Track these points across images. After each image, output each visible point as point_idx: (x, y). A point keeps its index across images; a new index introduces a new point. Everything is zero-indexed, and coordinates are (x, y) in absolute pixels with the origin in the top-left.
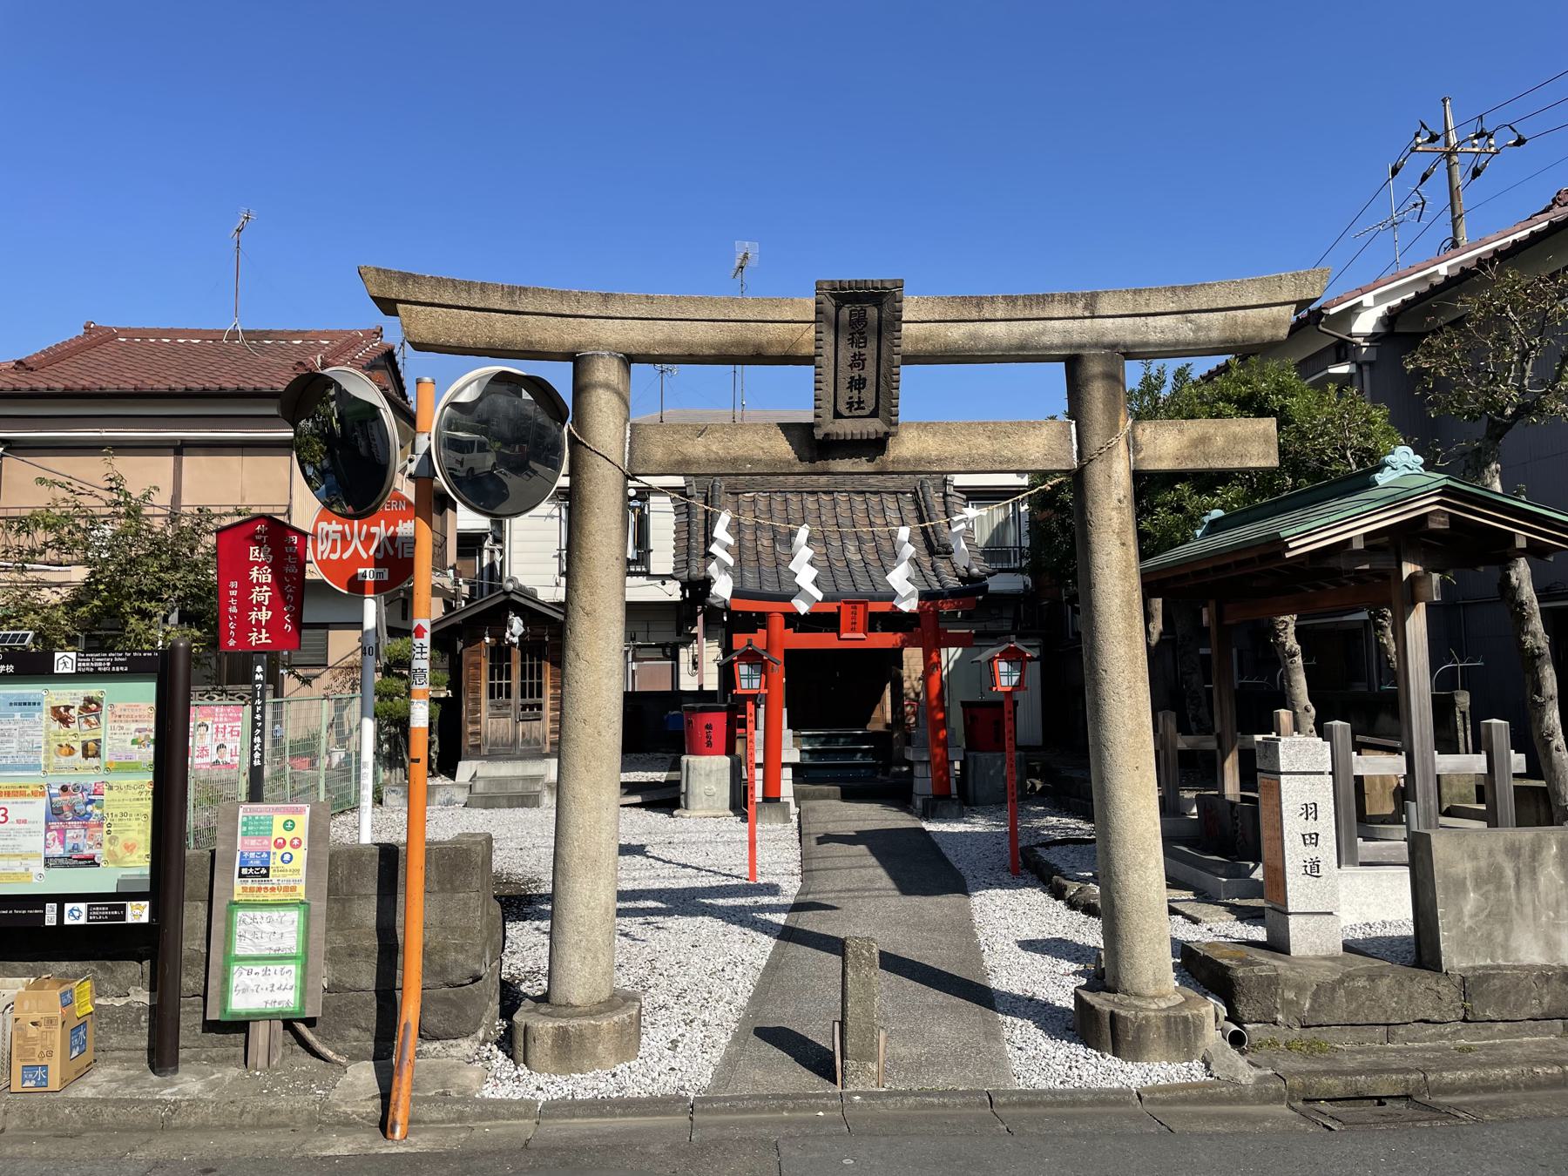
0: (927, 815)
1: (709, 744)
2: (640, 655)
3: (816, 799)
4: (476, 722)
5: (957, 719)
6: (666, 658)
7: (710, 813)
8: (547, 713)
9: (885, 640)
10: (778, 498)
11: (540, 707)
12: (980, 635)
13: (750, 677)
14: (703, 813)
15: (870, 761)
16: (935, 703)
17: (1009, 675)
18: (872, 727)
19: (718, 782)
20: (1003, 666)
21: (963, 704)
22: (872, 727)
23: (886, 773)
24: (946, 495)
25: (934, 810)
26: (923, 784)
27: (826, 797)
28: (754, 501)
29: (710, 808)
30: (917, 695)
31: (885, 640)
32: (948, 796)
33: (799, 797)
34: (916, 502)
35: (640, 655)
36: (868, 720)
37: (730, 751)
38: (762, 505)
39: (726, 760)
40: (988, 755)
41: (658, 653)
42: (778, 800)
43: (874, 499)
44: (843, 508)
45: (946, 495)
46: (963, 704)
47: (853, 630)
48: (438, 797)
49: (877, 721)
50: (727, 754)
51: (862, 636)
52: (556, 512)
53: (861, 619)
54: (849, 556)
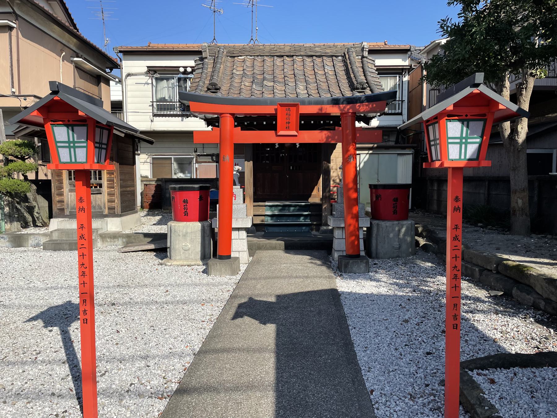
0: (345, 266)
1: (186, 214)
2: (199, 160)
3: (267, 249)
4: (61, 194)
5: (365, 195)
6: (213, 161)
7: (185, 263)
8: (105, 189)
9: (316, 137)
10: (259, 59)
11: (101, 186)
12: (378, 148)
13: (71, 145)
14: (181, 263)
15: (308, 222)
16: (351, 185)
17: (463, 142)
18: (312, 200)
19: (192, 241)
20: (454, 128)
21: (370, 186)
22: (312, 200)
23: (318, 230)
24: (363, 57)
25: (346, 266)
26: (340, 244)
27: (274, 248)
28: (244, 61)
29: (187, 259)
30: (340, 180)
31: (316, 137)
32: (358, 256)
33: (252, 250)
34: (344, 61)
35: (199, 160)
36: (310, 196)
37: (203, 218)
38: (248, 63)
39: (197, 226)
40: (388, 223)
41: (209, 159)
42: (229, 257)
43: (318, 60)
44: (313, 92)
45: (363, 57)
46: (370, 186)
47: (288, 129)
48: (30, 242)
49: (315, 196)
50: (200, 220)
51: (294, 133)
52: (150, 81)
53: (294, 120)
54: (298, 91)
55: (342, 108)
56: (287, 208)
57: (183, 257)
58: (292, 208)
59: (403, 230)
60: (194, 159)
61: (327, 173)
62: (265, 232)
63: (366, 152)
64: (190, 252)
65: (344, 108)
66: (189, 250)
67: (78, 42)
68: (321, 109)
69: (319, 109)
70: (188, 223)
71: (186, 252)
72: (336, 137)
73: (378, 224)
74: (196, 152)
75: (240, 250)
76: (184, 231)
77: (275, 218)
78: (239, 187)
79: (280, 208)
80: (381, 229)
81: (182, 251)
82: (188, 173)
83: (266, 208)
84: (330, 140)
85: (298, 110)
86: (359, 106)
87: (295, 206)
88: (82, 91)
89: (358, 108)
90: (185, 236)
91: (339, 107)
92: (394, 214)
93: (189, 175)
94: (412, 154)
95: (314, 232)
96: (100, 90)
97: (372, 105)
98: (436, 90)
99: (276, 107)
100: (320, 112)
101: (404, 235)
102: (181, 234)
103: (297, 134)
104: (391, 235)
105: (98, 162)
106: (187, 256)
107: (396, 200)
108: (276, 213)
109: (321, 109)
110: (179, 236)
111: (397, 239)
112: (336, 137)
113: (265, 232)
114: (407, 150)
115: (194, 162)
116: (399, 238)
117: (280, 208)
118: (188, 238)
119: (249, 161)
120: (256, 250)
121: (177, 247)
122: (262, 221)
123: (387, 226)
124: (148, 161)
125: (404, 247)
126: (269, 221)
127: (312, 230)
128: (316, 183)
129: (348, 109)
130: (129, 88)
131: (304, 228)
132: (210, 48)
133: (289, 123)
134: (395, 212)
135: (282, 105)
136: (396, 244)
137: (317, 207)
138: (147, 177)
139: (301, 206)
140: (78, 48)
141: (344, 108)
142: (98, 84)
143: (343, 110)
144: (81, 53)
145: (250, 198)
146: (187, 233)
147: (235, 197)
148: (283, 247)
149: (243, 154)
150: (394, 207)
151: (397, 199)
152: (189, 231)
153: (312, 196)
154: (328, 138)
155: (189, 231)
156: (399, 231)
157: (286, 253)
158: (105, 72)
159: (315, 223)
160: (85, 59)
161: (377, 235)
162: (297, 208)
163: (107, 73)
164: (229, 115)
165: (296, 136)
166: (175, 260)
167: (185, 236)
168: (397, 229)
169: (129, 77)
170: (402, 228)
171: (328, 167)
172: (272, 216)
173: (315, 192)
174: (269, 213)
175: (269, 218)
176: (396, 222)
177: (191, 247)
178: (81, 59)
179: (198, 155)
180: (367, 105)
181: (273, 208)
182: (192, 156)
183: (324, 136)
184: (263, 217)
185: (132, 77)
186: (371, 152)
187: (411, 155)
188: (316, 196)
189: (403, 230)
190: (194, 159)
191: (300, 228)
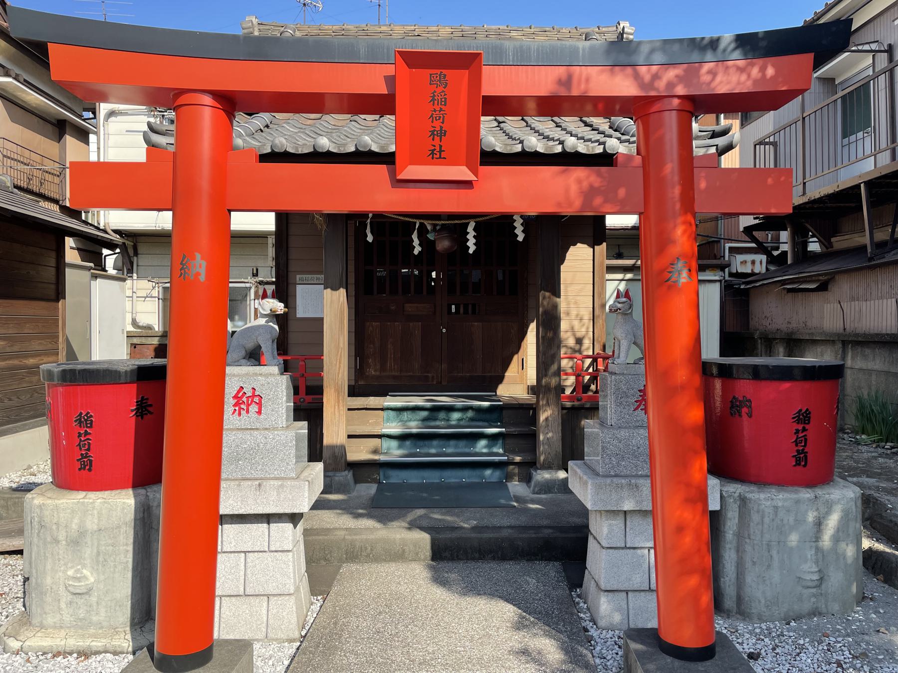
3: (377, 559)
7: (73, 643)
14: (57, 641)
19: (100, 561)
23: (527, 479)
27: (398, 556)
29: (81, 625)
33: (322, 567)
36: (500, 379)
47: (437, 156)
51: (462, 173)
55: (647, 78)
56: (442, 415)
57: (67, 618)
58: (456, 416)
59: (833, 521)
60: (252, 291)
61: (550, 323)
62: (379, 483)
63: (620, 276)
64: (94, 599)
65: (656, 77)
66: (89, 592)
67: (12, 50)
68: (567, 82)
69: (560, 82)
70: (92, 495)
71: (80, 601)
72: (622, 192)
73: (743, 501)
74: (255, 275)
75: (271, 590)
76: (74, 526)
77: (408, 443)
78: (275, 370)
79: (425, 414)
80: (755, 517)
81: (65, 597)
82: (240, 320)
83: (385, 413)
84: (598, 201)
85: (476, 81)
86: (713, 73)
87: (465, 409)
88: (351, 268)
89: (706, 78)
90: (76, 542)
91: (637, 77)
92: (798, 464)
93: (240, 323)
94: (720, 281)
95: (516, 487)
96: (63, 150)
97: (763, 69)
98: (770, 143)
99: (390, 70)
100: (563, 92)
101: (836, 539)
102: (62, 536)
103: (470, 177)
104: (793, 539)
105: (464, 313)
106: (82, 613)
107: (804, 418)
108: (414, 427)
109: (567, 82)
110: (56, 541)
111: (810, 553)
112: (622, 192)
113: (379, 483)
114: (708, 272)
115: (253, 297)
116: (818, 549)
117: (425, 414)
118: (88, 552)
119: (335, 288)
120: (341, 561)
121: (49, 581)
122: (375, 452)
123: (776, 508)
124: (155, 293)
125: (835, 579)
126: (394, 452)
127: (509, 477)
128: (517, 348)
129: (670, 85)
130: (112, 140)
131: (488, 472)
132: (262, 27)
133: (442, 133)
134: (801, 459)
135: (414, 60)
136: (809, 570)
137: (521, 416)
138: (149, 328)
139: (479, 410)
140: (10, 59)
141: (656, 77)
142: (60, 137)
143: (651, 85)
144: (16, 70)
145: (338, 391)
146: (82, 533)
147: (260, 404)
148: (427, 551)
149: (320, 273)
150: (796, 443)
151: (808, 413)
152: (91, 524)
153: (506, 380)
154: (589, 194)
155: (91, 524)
156: (819, 524)
157: (439, 580)
158: (80, 116)
159: (518, 459)
160: (27, 83)
161: (740, 536)
162: (470, 414)
163: (84, 120)
164: (207, 100)
165: (468, 184)
166: (42, 627)
167: (76, 542)
168: (811, 517)
169: (112, 119)
170: (828, 513)
171: (555, 307)
172: (402, 438)
173: (512, 372)
174: (394, 429)
175: (394, 443)
176: (806, 494)
177: (98, 581)
178: (10, 80)
179: (261, 283)
180: (741, 70)
181: (406, 415)
182: (248, 285)
183: (574, 189)
184: (377, 441)
185: (120, 118)
186: (629, 276)
187: (718, 285)
188: (518, 381)
189: (833, 521)
190: (252, 291)
191: (477, 472)
